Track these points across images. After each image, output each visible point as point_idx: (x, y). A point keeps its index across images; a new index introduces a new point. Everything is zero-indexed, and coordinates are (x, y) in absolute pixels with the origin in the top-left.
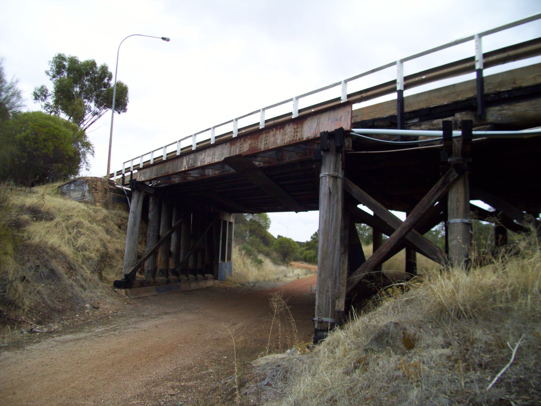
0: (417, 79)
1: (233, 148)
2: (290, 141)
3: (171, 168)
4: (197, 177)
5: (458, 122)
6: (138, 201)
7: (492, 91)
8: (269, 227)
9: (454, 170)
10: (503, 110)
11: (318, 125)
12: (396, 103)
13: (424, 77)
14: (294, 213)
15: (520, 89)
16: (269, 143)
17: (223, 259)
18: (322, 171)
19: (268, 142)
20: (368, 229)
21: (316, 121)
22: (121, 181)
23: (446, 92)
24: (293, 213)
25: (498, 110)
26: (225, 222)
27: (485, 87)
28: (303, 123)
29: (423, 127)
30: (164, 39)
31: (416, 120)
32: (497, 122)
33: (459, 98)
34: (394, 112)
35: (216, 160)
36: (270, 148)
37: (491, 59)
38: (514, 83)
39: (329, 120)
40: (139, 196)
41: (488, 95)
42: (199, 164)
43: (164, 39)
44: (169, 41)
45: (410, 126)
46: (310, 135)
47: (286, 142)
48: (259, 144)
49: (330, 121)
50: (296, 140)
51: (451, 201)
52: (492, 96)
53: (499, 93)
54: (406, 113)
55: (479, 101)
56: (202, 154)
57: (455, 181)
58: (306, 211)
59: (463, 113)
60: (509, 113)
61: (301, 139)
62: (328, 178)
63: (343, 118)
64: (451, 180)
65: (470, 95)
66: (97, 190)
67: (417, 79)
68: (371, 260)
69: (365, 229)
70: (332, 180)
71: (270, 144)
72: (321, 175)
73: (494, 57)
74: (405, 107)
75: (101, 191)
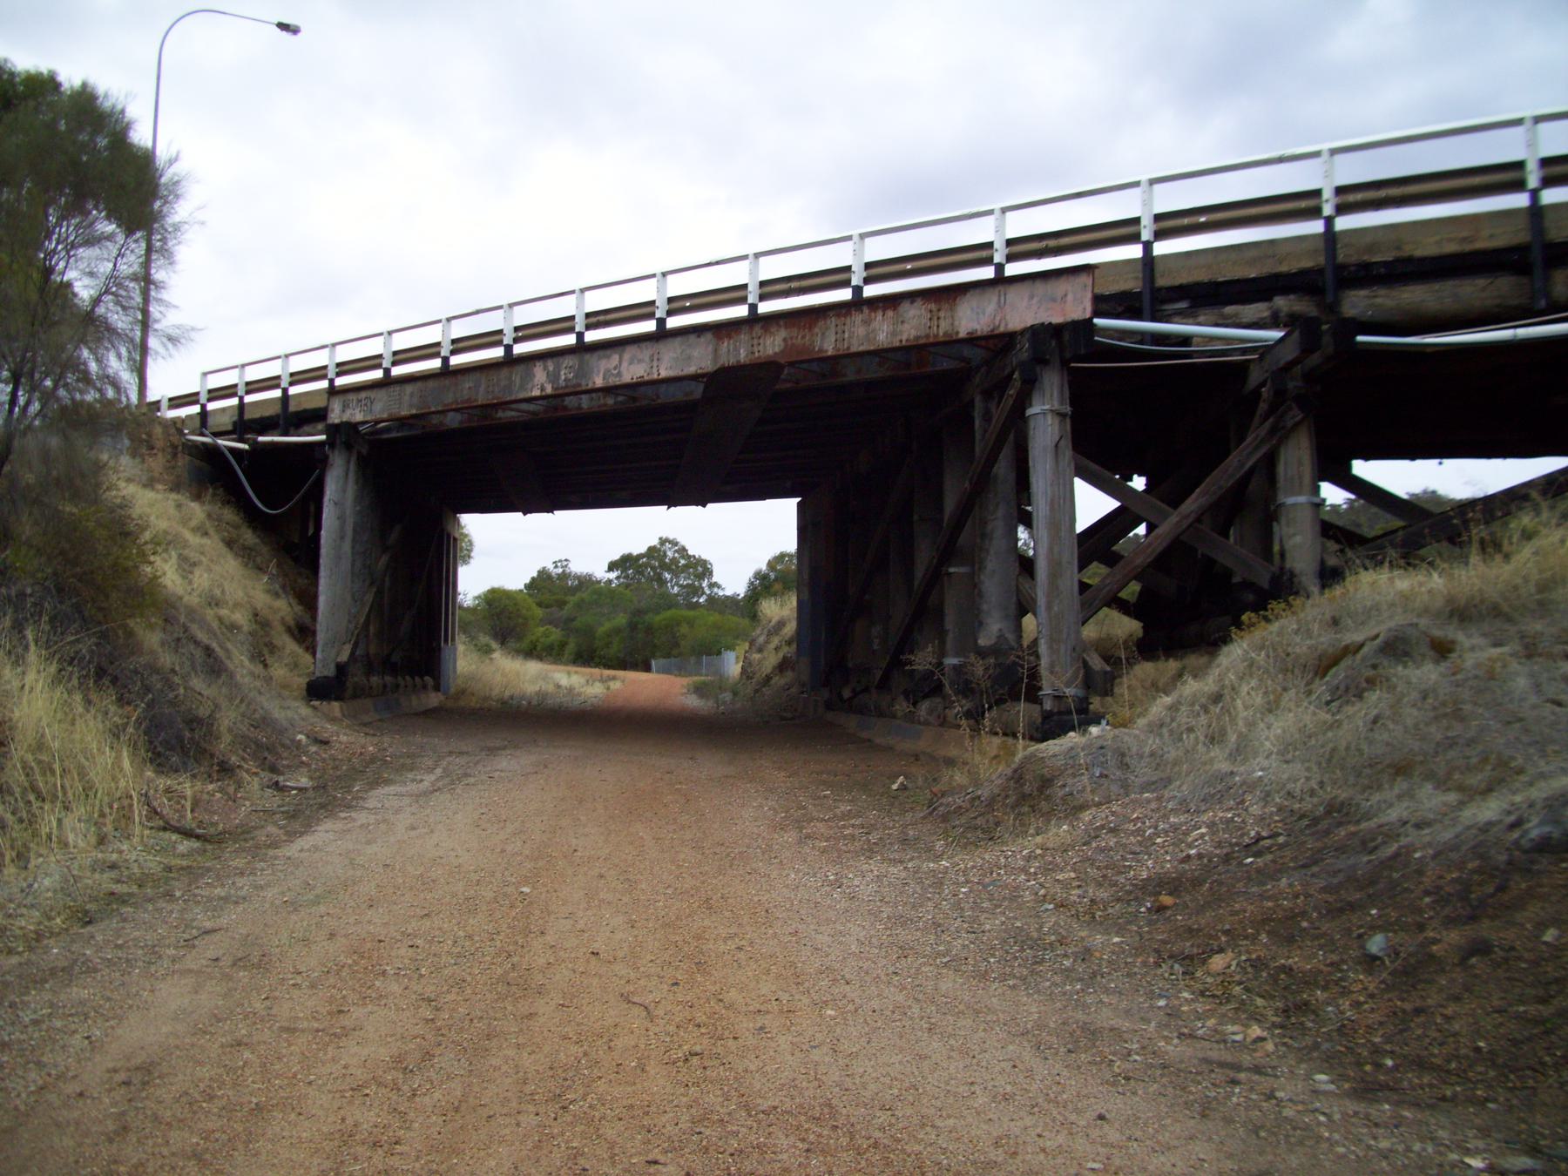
0: (1186, 221)
1: (725, 345)
2: (917, 338)
3: (482, 389)
4: (533, 413)
5: (1282, 314)
6: (347, 474)
7: (1354, 259)
8: (469, 557)
9: (1294, 405)
10: (1375, 297)
11: (1000, 307)
12: (1140, 267)
13: (1203, 219)
14: (520, 514)
15: (1410, 260)
16: (850, 337)
17: (446, 641)
18: (1034, 402)
19: (846, 335)
20: (684, 565)
21: (995, 299)
22: (197, 423)
23: (1253, 253)
24: (517, 516)
25: (1368, 297)
26: (449, 536)
27: (1339, 251)
28: (955, 299)
29: (1201, 319)
30: (283, 27)
31: (1183, 305)
32: (1363, 319)
33: (1284, 268)
34: (1132, 284)
35: (664, 374)
36: (854, 349)
37: (1351, 198)
38: (1398, 248)
39: (1031, 297)
40: (348, 462)
41: (1343, 267)
42: (599, 382)
43: (283, 27)
44: (300, 35)
45: (1170, 315)
46: (978, 327)
47: (904, 338)
48: (818, 339)
49: (1035, 300)
50: (936, 336)
51: (1286, 464)
52: (1352, 268)
53: (1366, 266)
54: (1160, 289)
55: (1329, 277)
56: (609, 357)
57: (1297, 425)
58: (550, 510)
59: (1292, 297)
60: (1389, 303)
61: (951, 335)
62: (1049, 417)
63: (1070, 297)
64: (1290, 424)
65: (1307, 263)
66: (153, 448)
67: (1186, 221)
68: (1108, 581)
69: (678, 567)
70: (1057, 420)
71: (854, 341)
72: (1029, 412)
73: (1359, 196)
74: (1157, 275)
75: (163, 450)
